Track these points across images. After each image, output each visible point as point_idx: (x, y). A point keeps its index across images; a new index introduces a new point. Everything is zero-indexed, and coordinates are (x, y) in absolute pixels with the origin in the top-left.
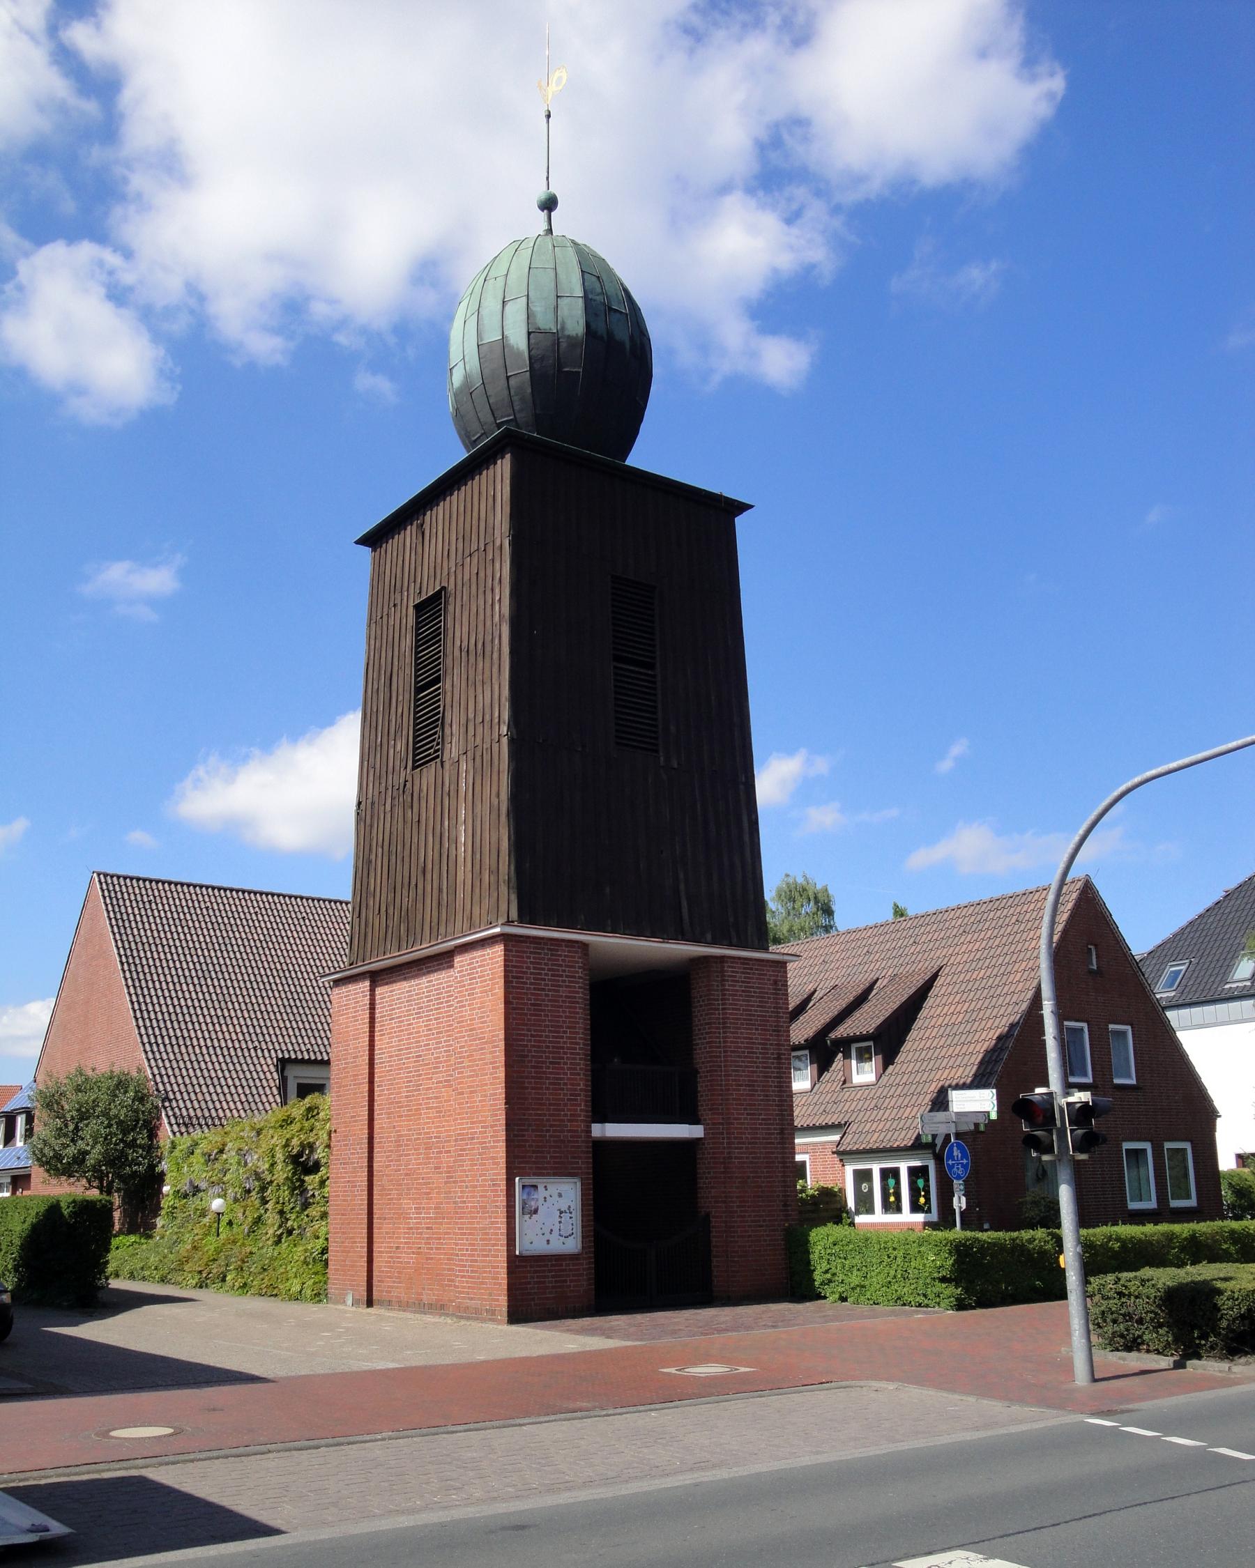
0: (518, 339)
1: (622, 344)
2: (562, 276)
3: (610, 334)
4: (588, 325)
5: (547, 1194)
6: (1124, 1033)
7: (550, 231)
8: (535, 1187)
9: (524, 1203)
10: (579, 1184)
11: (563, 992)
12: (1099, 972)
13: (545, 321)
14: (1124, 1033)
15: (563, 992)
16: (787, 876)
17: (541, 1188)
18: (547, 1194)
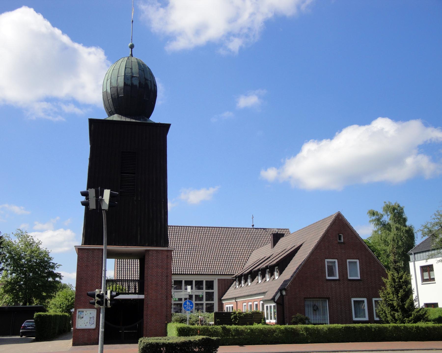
0: (109, 91)
1: (136, 86)
2: (120, 71)
3: (132, 84)
4: (125, 83)
5: (86, 313)
6: (356, 262)
7: (132, 55)
8: (83, 311)
9: (79, 316)
10: (96, 311)
11: (95, 262)
12: (344, 243)
13: (114, 84)
14: (356, 262)
15: (95, 262)
16: (385, 202)
17: (85, 312)
18: (86, 313)
